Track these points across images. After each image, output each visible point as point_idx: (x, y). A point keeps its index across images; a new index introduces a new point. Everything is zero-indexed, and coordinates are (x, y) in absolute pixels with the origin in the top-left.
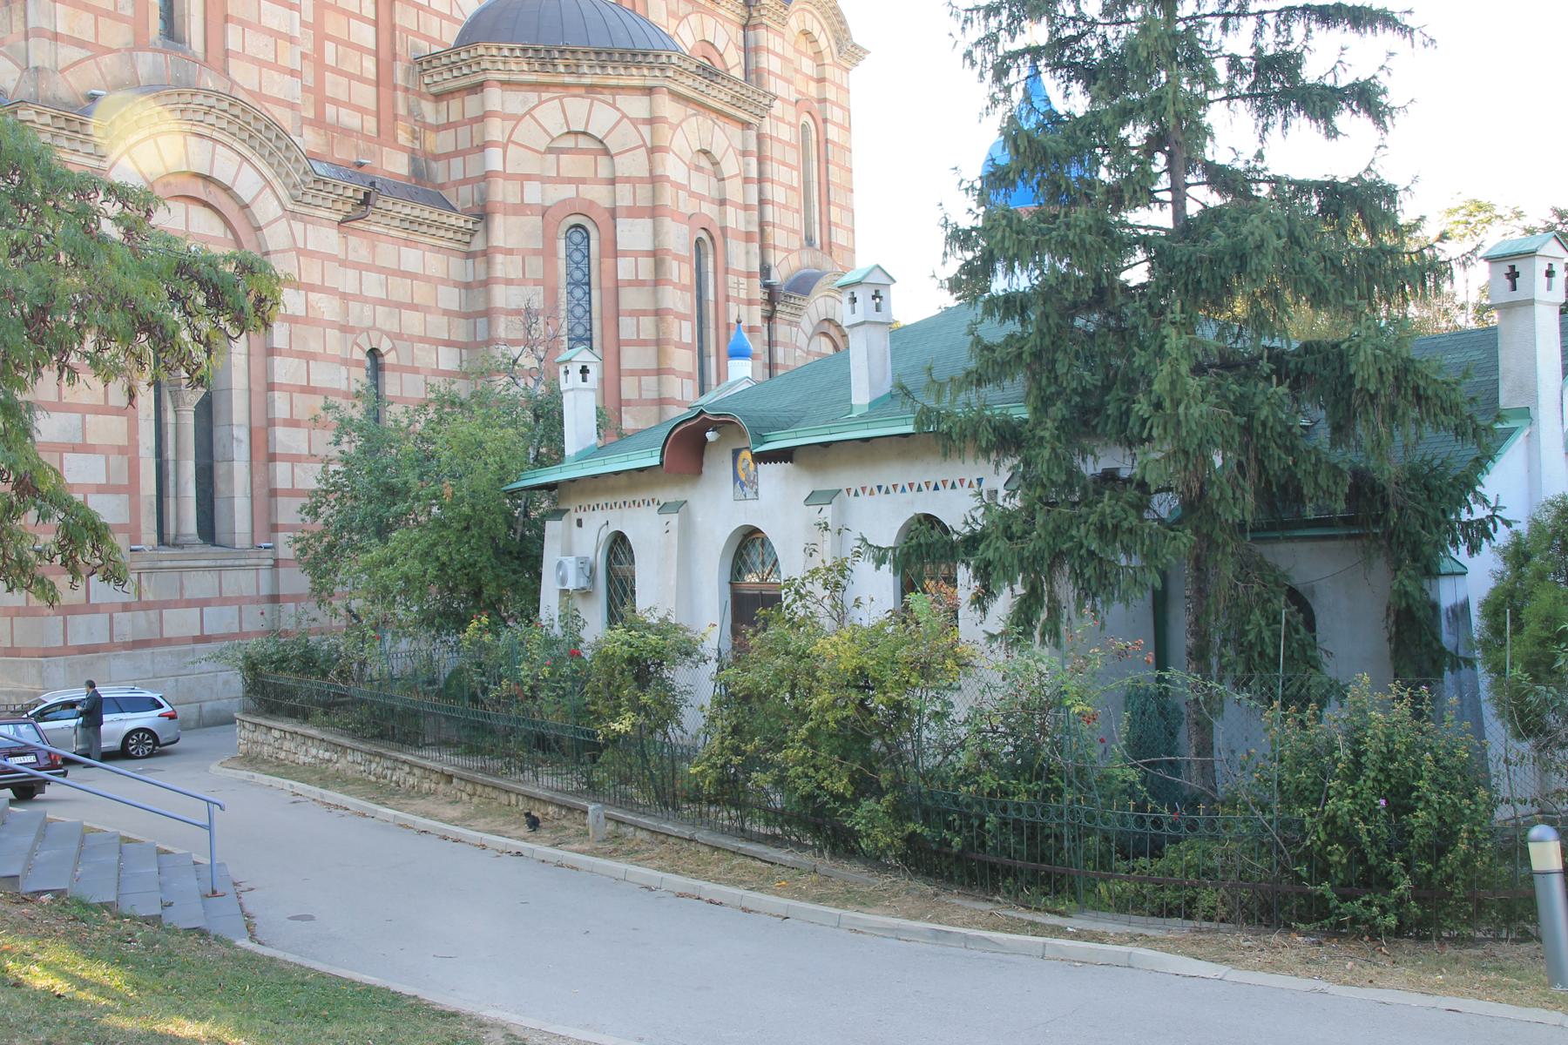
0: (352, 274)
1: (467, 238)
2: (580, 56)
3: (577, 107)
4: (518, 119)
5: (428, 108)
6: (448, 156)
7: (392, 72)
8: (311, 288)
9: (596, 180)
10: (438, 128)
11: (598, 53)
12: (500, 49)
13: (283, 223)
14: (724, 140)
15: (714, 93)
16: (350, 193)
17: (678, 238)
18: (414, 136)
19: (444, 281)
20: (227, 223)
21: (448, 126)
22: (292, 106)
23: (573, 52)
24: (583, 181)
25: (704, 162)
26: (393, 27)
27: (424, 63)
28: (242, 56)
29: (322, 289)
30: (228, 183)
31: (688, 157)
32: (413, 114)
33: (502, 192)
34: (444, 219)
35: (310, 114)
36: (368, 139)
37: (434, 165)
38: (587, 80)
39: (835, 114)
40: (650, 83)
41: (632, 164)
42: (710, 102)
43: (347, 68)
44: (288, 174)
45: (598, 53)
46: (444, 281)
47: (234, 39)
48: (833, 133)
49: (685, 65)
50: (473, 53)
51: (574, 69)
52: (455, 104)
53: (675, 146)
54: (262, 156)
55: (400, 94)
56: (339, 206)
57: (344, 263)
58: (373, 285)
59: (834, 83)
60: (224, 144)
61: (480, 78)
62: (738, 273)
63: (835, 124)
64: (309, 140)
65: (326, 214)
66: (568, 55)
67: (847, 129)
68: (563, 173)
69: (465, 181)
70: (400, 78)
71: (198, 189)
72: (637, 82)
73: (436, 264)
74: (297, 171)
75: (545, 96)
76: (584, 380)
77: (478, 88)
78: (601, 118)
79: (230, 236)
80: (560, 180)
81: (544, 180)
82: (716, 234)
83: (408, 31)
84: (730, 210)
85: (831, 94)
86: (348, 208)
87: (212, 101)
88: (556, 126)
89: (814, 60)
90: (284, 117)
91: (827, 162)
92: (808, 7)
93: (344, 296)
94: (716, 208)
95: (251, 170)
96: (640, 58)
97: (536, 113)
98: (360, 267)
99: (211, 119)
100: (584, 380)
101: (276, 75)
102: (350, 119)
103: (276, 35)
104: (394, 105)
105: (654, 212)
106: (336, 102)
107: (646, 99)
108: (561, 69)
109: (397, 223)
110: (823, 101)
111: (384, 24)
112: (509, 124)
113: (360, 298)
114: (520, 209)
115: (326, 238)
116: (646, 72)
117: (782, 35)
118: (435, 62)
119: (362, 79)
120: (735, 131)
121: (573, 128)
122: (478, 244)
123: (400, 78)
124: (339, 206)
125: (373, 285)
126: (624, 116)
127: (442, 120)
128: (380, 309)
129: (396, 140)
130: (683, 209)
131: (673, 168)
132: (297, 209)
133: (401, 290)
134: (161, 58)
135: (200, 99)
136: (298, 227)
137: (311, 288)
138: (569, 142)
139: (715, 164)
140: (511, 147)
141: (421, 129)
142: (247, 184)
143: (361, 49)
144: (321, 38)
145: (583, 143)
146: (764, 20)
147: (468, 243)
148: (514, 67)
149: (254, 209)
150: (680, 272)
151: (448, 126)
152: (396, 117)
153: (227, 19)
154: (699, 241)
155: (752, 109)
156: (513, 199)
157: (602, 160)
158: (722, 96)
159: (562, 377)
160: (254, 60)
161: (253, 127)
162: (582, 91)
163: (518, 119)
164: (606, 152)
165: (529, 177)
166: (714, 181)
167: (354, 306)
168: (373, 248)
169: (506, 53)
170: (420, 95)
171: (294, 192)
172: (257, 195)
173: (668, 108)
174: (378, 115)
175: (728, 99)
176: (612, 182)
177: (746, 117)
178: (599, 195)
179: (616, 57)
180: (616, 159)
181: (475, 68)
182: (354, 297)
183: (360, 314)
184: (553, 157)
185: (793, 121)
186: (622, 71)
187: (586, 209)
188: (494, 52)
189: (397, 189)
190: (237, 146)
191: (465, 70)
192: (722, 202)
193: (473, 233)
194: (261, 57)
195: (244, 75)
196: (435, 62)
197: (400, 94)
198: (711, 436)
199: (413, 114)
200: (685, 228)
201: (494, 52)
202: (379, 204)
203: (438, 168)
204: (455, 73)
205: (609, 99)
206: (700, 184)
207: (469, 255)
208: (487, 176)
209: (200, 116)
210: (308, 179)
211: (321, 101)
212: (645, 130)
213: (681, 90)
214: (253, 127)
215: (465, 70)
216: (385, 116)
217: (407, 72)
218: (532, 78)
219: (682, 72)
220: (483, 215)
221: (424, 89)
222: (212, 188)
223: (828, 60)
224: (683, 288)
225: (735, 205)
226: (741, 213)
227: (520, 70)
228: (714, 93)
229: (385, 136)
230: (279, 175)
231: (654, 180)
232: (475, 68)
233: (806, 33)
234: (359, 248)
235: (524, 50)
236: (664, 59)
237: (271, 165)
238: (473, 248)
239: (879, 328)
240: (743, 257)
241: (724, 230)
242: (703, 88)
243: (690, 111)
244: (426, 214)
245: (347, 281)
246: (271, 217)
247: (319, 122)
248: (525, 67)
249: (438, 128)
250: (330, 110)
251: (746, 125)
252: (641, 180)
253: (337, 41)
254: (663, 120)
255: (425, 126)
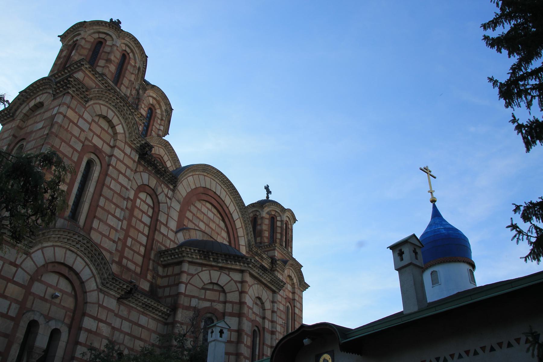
0: (118, 320)
1: (166, 317)
2: (219, 255)
3: (215, 274)
4: (193, 275)
5: (160, 269)
6: (165, 287)
7: (150, 254)
8: (101, 321)
9: (219, 302)
10: (162, 277)
11: (225, 255)
12: (190, 249)
13: (96, 292)
14: (266, 295)
15: (265, 277)
16: (125, 287)
17: (247, 327)
18: (153, 277)
19: (155, 332)
20: (74, 288)
21: (167, 276)
22: (111, 253)
23: (217, 254)
24: (214, 301)
25: (258, 302)
26: (153, 239)
27: (161, 253)
28: (97, 230)
29: (105, 322)
30: (78, 271)
31: (254, 298)
32: (155, 270)
33: (183, 301)
34: (159, 307)
35: (117, 259)
36: (136, 274)
37: (159, 290)
38: (220, 265)
39: (298, 305)
40: (243, 268)
41: (233, 297)
42: (263, 280)
43: (134, 248)
44: (102, 274)
45: (225, 255)
46: (155, 332)
47: (95, 224)
48: (297, 311)
49: (256, 264)
50: (180, 250)
51: (216, 260)
52: (170, 269)
53: (249, 293)
54: (94, 265)
55: (151, 262)
56: (120, 291)
57: (116, 315)
58: (126, 327)
59: (297, 294)
60: (81, 257)
61: (181, 259)
62: (267, 346)
63: (297, 308)
64: (115, 268)
65: (114, 293)
66: (215, 255)
67: (301, 310)
68: (207, 297)
69: (169, 296)
70: (152, 256)
71: (65, 271)
72: (238, 267)
73: (152, 325)
74: (106, 273)
75: (204, 269)
76: (221, 336)
77: (180, 263)
78: (224, 279)
79: (73, 293)
80: (205, 300)
81: (200, 299)
82: (261, 329)
83: (158, 242)
84: (267, 322)
85: (297, 298)
86: (123, 293)
87: (81, 239)
88: (206, 280)
89: (292, 286)
90: (107, 255)
91: (295, 320)
92: (291, 268)
93: (114, 328)
94: (261, 320)
95: (89, 270)
96: (240, 259)
97: (200, 274)
98: (122, 318)
99: (78, 246)
100: (221, 336)
101: (107, 240)
102: (131, 266)
103: (111, 227)
104: (148, 265)
105: (240, 315)
106: (127, 259)
107: (240, 275)
108: (212, 259)
109: (141, 304)
110: (294, 300)
111: (151, 237)
112: (189, 277)
113: (120, 331)
114: (188, 308)
115: (111, 303)
116: (242, 264)
117: (282, 275)
118: (166, 253)
119: (138, 254)
120: (270, 294)
121: (213, 281)
122: (170, 320)
123: (152, 256)
124: (120, 291)
125: (126, 327)
126: (232, 279)
127: (165, 274)
128: (127, 337)
129: (146, 276)
130: (250, 316)
131: (249, 300)
132: (103, 288)
133: (137, 331)
134: (66, 222)
135: (76, 237)
136: (101, 296)
137: (101, 321)
138: (211, 287)
139: (263, 303)
140: (189, 285)
141: (156, 275)
142: (86, 274)
143: (141, 244)
144: (127, 236)
145: (216, 287)
146: (277, 269)
147: (166, 319)
148: (194, 256)
149: (86, 284)
150: (247, 340)
151: (167, 276)
152: (148, 269)
153: (95, 217)
154: (254, 331)
155: (277, 286)
156: (186, 304)
157: (222, 295)
158: (267, 279)
159: (209, 334)
160: (101, 233)
161: (94, 254)
162: (218, 269)
163: (193, 275)
164: (224, 291)
165: (194, 297)
166: (261, 310)
167: (117, 333)
168: (129, 313)
169: (192, 251)
170: (158, 264)
171: (103, 281)
172: (88, 279)
173: (248, 278)
174: (142, 267)
175: (269, 280)
176: (225, 302)
177: (274, 289)
178: (219, 307)
179: (232, 257)
180: (227, 294)
181: (180, 255)
182: (117, 329)
183: (118, 337)
184: (203, 291)
185: (284, 304)
186: (233, 263)
187: (213, 311)
188: (188, 250)
189: (143, 293)
190: (86, 259)
191: (176, 256)
192: (264, 318)
193: (169, 315)
194: (104, 233)
195: (95, 237)
196: (166, 253)
197: (151, 262)
198: (306, 341)
199: (155, 270)
200: (250, 324)
201: (188, 250)
202: (135, 295)
203: (160, 291)
204: (173, 257)
205: (227, 273)
206: (256, 309)
207: (166, 324)
208: (179, 294)
209: (74, 244)
210: (110, 277)
211: (122, 257)
212: (239, 285)
213: (253, 273)
214: (94, 254)
215: (176, 256)
216: (144, 268)
217: (155, 255)
218: (200, 261)
219: (255, 266)
220: (174, 308)
221: (160, 262)
222: (71, 273)
223: (296, 287)
224: (248, 347)
225: (268, 319)
226: (270, 324)
227: (197, 258)
228: (265, 277)
229: (143, 275)
230: (99, 273)
231: (241, 303)
232: (180, 255)
233: (289, 276)
234: (124, 312)
235: (199, 251)
236: (249, 260)
237: (97, 269)
238: (168, 321)
239: (407, 269)
240: (270, 340)
241: (264, 328)
242: (261, 274)
243: (255, 282)
244: (152, 303)
245: (117, 323)
246: (92, 289)
247: (119, 263)
248: (198, 257)
249: (162, 277)
250: (124, 261)
251: (274, 292)
252: (236, 303)
253: (133, 239)
254: (246, 282)
255: (158, 275)
